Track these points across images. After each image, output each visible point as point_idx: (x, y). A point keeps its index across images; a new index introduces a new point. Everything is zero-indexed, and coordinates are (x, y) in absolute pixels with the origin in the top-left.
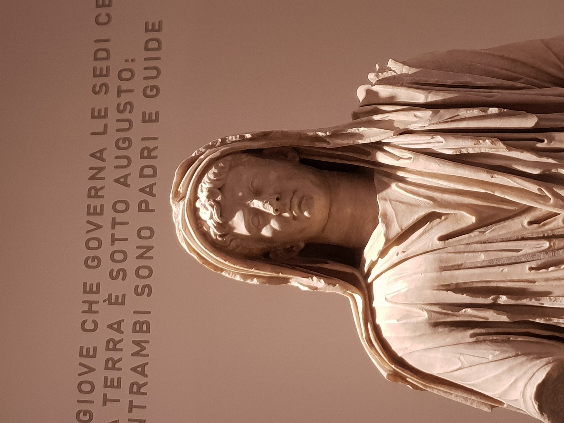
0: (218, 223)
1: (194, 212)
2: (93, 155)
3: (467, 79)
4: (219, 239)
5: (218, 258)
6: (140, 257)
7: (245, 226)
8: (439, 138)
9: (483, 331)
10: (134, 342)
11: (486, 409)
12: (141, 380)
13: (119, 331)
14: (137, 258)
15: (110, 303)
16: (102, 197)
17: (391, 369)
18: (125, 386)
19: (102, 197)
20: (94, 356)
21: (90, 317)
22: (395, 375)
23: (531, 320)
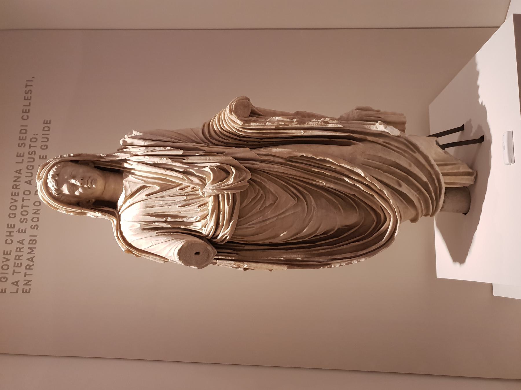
0: (56, 189)
1: (46, 184)
2: (16, 172)
3: (161, 138)
4: (56, 195)
5: (55, 204)
6: (34, 213)
7: (68, 191)
8: (147, 157)
9: (161, 231)
10: (29, 248)
11: (162, 262)
12: (31, 263)
13: (22, 244)
14: (33, 214)
15: (19, 232)
16: (19, 189)
17: (126, 248)
18: (24, 266)
19: (19, 189)
20: (10, 254)
21: (9, 238)
22: (128, 251)
23: (179, 227)
